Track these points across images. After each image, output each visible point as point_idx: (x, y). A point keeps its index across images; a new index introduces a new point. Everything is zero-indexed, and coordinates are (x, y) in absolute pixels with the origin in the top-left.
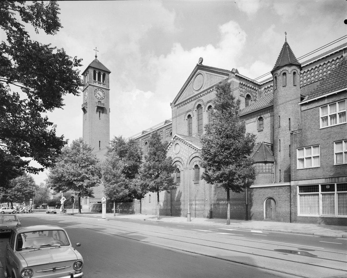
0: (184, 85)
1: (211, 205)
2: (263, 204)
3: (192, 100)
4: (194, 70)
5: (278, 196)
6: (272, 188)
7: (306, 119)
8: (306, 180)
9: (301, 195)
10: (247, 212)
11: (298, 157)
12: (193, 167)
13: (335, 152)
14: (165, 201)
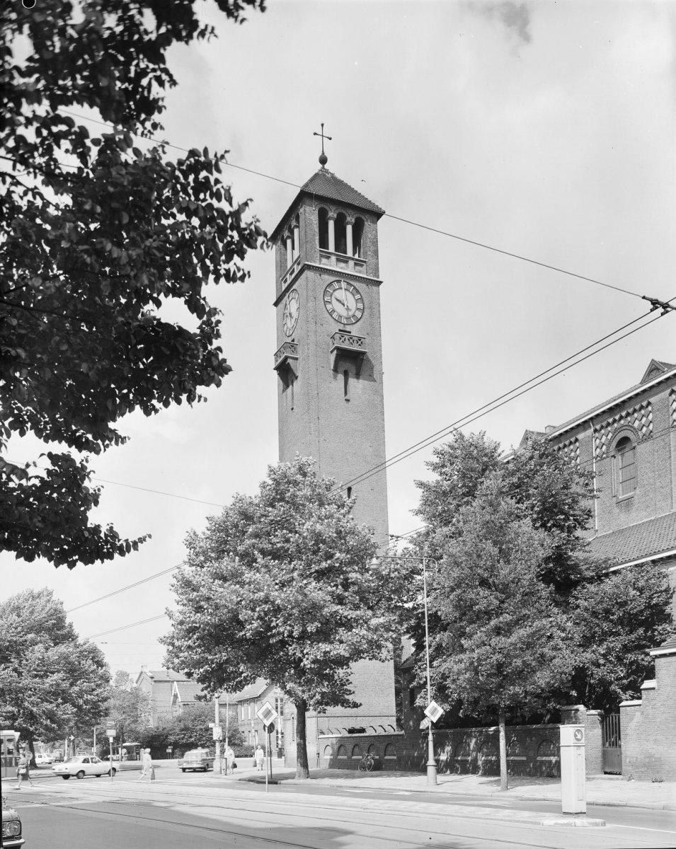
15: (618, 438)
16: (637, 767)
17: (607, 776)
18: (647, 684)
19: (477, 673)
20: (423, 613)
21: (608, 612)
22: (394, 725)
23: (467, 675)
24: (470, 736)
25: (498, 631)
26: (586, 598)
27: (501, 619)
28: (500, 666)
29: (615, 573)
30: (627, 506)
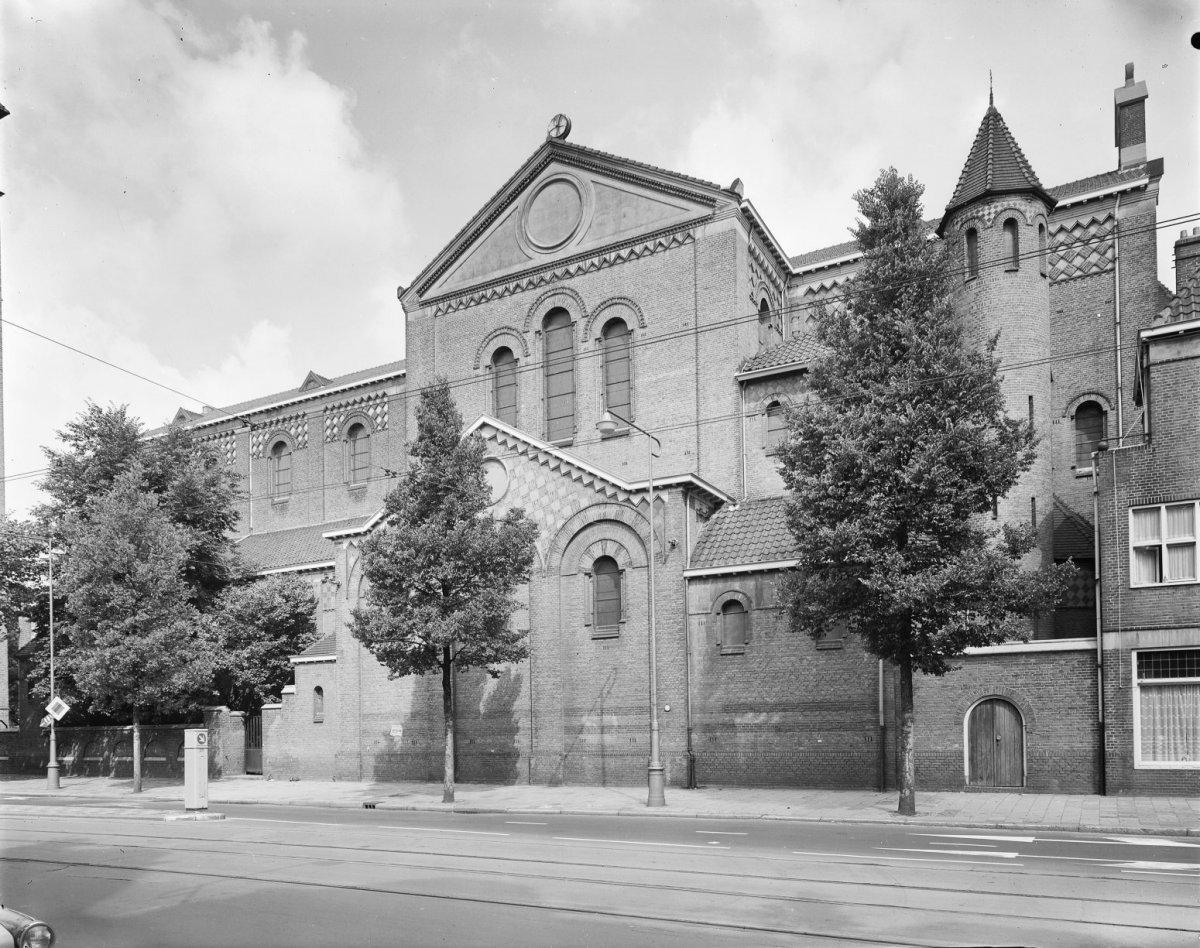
0: (475, 219)
1: (689, 731)
2: (962, 724)
3: (518, 286)
4: (530, 162)
5: (1034, 690)
6: (1006, 661)
7: (1170, 394)
8: (1174, 631)
9: (1144, 688)
10: (883, 755)
11: (1135, 540)
12: (588, 564)
13: (1132, 545)
14: (414, 715)
15: (275, 441)
16: (276, 767)
17: (249, 776)
18: (287, 689)
19: (109, 670)
20: (47, 597)
21: (254, 617)
22: (6, 720)
23: (98, 673)
24: (102, 736)
25: (133, 630)
26: (234, 600)
27: (137, 618)
28: (135, 665)
29: (263, 577)
30: (282, 509)
